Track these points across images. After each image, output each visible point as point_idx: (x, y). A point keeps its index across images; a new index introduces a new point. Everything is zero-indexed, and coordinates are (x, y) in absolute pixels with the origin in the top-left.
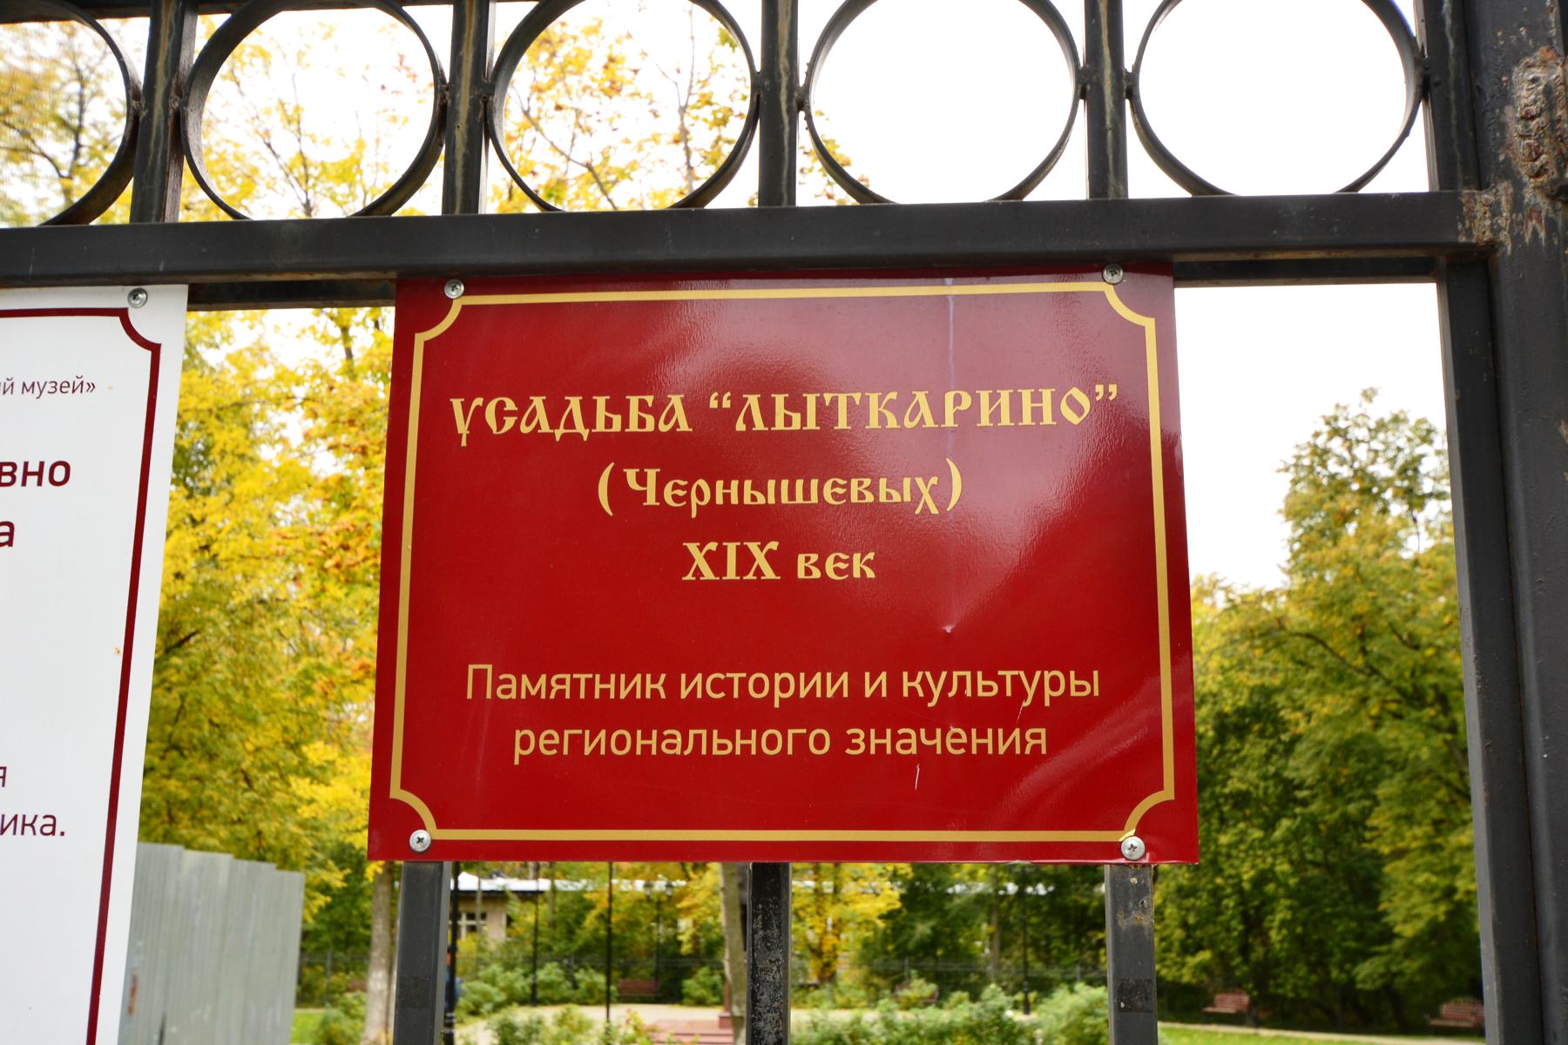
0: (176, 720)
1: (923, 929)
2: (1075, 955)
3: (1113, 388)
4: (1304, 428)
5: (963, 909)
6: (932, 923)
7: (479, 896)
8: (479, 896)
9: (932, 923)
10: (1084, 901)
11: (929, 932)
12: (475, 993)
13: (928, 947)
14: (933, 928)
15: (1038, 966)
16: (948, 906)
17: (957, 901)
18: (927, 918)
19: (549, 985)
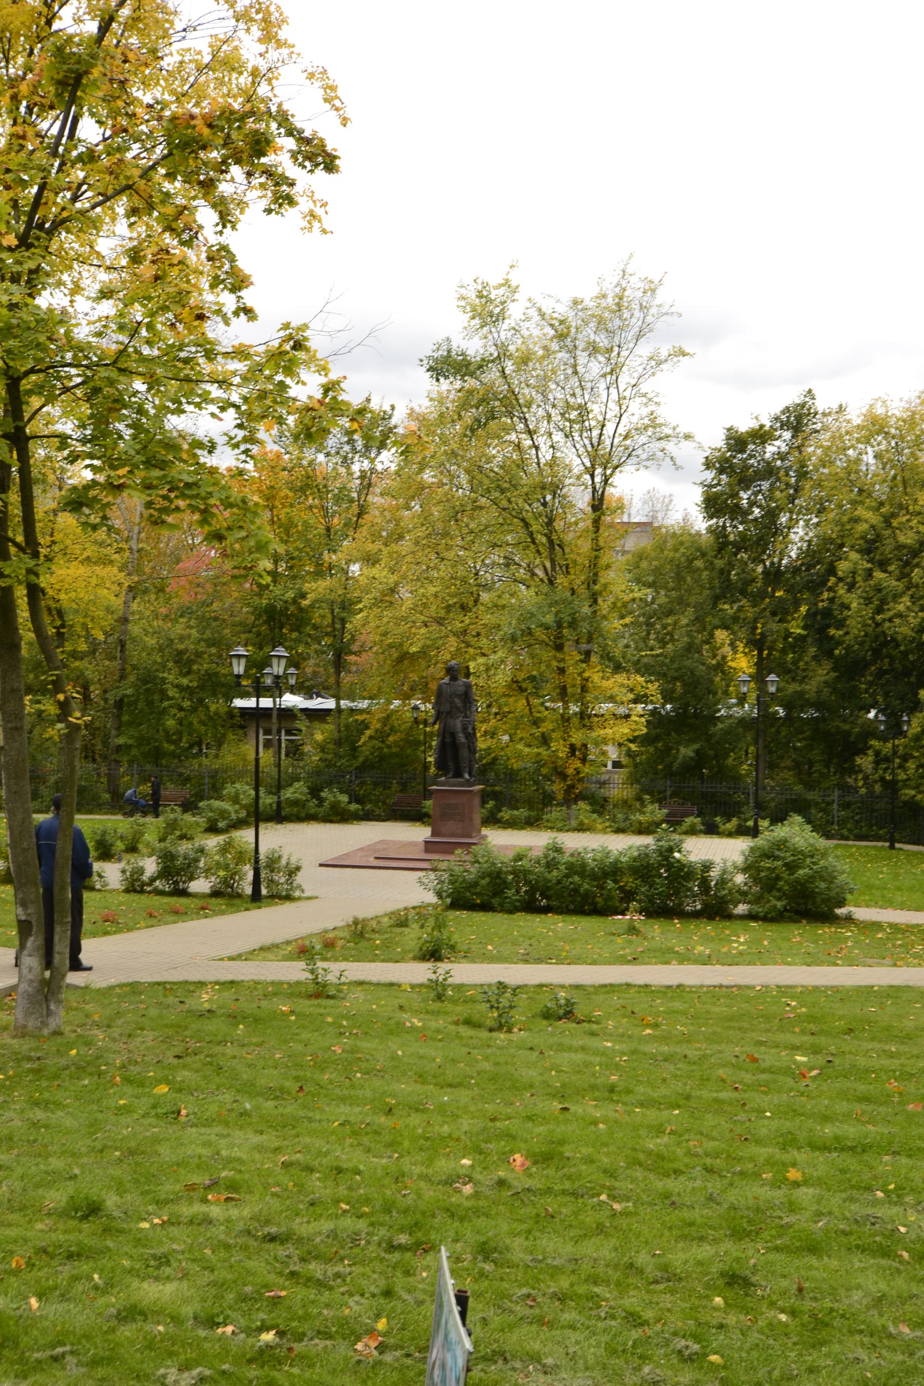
0: (660, 439)
1: (686, 752)
2: (835, 779)
3: (241, 651)
4: (552, 283)
5: (728, 732)
6: (696, 746)
7: (275, 713)
8: (275, 713)
9: (696, 746)
10: (846, 727)
11: (692, 754)
12: (211, 811)
13: (693, 768)
14: (697, 752)
15: (799, 788)
16: (713, 730)
17: (720, 726)
18: (691, 741)
19: (295, 803)
